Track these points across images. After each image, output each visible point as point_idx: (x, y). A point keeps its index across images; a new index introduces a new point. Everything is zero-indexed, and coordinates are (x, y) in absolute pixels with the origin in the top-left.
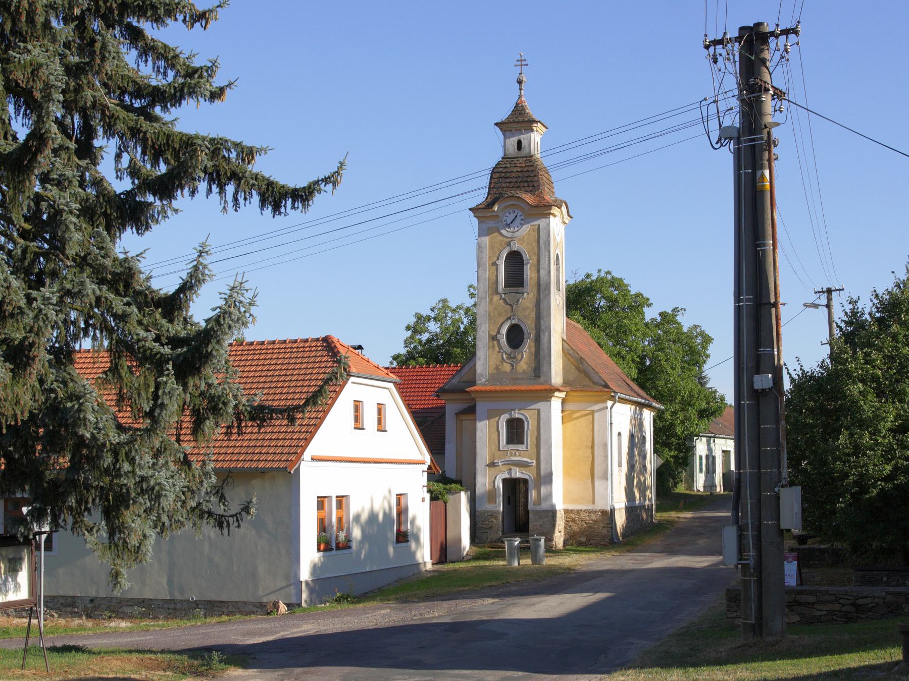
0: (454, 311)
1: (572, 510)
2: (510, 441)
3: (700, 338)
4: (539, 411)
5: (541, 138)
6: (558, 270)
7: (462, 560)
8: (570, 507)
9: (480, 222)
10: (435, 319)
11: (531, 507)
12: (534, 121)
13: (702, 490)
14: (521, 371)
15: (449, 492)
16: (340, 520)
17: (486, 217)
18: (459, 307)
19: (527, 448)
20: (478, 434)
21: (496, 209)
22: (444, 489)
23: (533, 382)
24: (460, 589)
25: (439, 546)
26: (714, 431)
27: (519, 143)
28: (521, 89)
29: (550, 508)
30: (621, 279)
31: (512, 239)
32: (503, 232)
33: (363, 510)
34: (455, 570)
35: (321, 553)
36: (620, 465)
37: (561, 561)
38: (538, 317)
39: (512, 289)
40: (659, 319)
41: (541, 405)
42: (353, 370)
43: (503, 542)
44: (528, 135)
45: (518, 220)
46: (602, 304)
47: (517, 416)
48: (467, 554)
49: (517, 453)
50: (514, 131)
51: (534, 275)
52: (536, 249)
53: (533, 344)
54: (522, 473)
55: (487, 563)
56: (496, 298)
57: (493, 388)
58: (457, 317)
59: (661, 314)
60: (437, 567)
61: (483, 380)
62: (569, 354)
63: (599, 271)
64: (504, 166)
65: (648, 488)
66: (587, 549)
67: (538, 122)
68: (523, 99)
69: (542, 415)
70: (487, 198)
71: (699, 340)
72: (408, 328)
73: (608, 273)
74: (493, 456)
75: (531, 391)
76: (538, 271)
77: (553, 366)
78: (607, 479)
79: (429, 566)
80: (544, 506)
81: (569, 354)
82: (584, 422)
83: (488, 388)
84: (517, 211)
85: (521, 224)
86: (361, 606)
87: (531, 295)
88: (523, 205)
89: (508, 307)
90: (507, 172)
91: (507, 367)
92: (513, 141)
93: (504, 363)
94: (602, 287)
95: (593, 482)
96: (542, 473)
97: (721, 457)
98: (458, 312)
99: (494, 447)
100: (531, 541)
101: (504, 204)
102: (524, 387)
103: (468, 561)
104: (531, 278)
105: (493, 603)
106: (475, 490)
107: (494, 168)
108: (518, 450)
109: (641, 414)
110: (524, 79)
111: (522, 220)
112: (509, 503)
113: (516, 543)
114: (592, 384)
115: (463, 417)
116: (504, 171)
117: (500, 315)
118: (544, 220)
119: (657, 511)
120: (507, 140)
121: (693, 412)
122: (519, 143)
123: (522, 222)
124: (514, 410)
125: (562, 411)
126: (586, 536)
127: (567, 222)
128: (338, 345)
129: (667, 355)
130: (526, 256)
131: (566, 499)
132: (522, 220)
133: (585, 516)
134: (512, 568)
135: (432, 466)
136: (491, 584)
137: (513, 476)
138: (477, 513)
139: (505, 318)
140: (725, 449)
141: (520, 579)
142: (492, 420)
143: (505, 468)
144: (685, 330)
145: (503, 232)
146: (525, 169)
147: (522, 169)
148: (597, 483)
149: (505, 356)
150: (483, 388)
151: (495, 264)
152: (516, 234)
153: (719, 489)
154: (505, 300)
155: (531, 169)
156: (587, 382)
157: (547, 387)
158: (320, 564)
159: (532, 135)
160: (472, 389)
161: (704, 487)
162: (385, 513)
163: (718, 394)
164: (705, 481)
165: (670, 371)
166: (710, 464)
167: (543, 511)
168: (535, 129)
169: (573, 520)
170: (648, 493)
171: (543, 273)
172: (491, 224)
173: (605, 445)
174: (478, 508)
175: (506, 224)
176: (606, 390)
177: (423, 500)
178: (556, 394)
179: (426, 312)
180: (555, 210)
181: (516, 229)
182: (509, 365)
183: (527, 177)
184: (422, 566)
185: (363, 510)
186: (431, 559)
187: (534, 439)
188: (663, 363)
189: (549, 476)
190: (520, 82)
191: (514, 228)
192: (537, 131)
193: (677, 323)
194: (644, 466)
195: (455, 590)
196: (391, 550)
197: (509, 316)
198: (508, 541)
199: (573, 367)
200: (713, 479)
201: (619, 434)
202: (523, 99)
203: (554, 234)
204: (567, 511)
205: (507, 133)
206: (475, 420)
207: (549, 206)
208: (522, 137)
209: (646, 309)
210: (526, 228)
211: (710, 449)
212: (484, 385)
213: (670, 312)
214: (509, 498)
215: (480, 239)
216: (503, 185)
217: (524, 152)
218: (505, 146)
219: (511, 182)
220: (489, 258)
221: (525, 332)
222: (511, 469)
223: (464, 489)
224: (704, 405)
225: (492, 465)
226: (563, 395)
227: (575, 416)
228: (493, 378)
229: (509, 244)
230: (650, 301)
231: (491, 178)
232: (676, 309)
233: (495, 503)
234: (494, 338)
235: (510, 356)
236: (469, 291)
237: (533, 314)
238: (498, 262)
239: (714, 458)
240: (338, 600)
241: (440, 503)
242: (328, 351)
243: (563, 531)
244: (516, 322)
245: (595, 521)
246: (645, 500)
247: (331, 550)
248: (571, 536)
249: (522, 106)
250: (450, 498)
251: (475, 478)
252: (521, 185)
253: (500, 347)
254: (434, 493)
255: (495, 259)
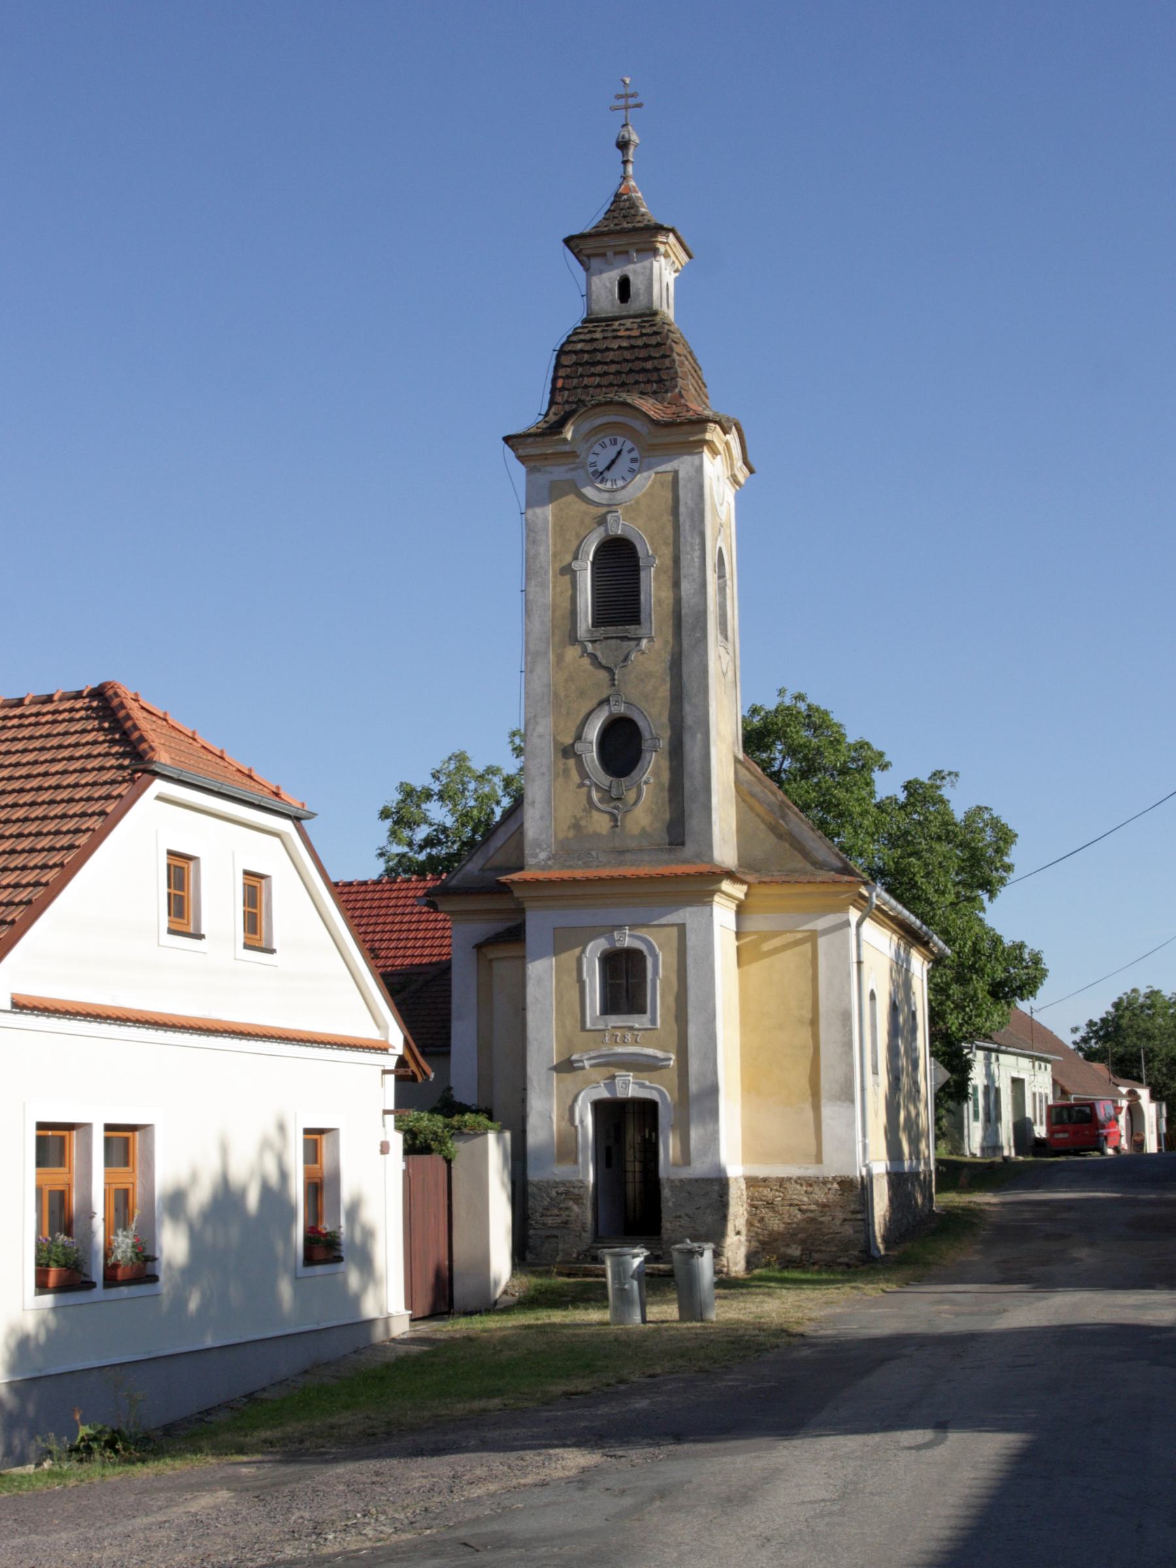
0: (481, 778)
1: (765, 1180)
2: (611, 1006)
3: (989, 831)
4: (682, 928)
5: (676, 280)
6: (722, 590)
7: (490, 1307)
8: (761, 1171)
9: (531, 471)
10: (441, 797)
11: (663, 1173)
12: (659, 229)
13: (978, 1153)
14: (636, 831)
15: (459, 1132)
16: (121, 1201)
17: (545, 457)
18: (492, 771)
19: (653, 1021)
20: (531, 1017)
21: (569, 436)
22: (446, 1126)
23: (665, 856)
24: (478, 1404)
25: (431, 1278)
26: (999, 1041)
27: (624, 285)
28: (625, 162)
29: (713, 1175)
30: (826, 713)
31: (611, 507)
32: (589, 491)
33: (194, 1178)
34: (469, 1339)
35: (48, 1300)
36: (875, 1072)
37: (752, 1308)
38: (677, 697)
39: (611, 630)
40: (902, 797)
41: (687, 915)
42: (163, 758)
43: (597, 1260)
44: (646, 263)
45: (624, 462)
46: (786, 764)
47: (628, 942)
48: (505, 1292)
49: (629, 1036)
50: (610, 254)
51: (667, 594)
52: (669, 530)
53: (665, 764)
54: (642, 1086)
55: (557, 1317)
56: (572, 652)
57: (566, 874)
58: (487, 790)
59: (908, 787)
60: (425, 1328)
61: (543, 855)
62: (753, 795)
63: (781, 692)
64: (588, 337)
65: (923, 1136)
66: (808, 1276)
67: (672, 230)
68: (632, 183)
69: (692, 940)
70: (546, 415)
71: (989, 836)
72: (385, 814)
73: (800, 697)
74: (568, 1044)
75: (663, 878)
76: (676, 584)
77: (715, 817)
78: (852, 1101)
79: (401, 1327)
80: (699, 1168)
81: (753, 795)
82: (792, 960)
83: (555, 874)
84: (620, 440)
85: (632, 471)
86: (144, 1472)
87: (658, 644)
88: (638, 425)
89: (603, 675)
90: (595, 350)
91: (600, 823)
92: (606, 282)
93: (595, 814)
94: (788, 725)
95: (817, 1108)
96: (693, 1087)
97: (1009, 1090)
98: (489, 781)
99: (571, 1023)
100: (675, 1255)
101: (587, 426)
102: (644, 870)
103: (507, 1310)
104: (659, 602)
105: (583, 1479)
106: (524, 1132)
107: (563, 345)
108: (631, 1028)
109: (908, 954)
110: (634, 137)
111: (633, 460)
112: (608, 1164)
113: (637, 1262)
114: (809, 867)
115: (493, 953)
116: (588, 347)
117: (582, 694)
118: (687, 459)
119: (937, 1192)
120: (595, 280)
121: (980, 986)
122: (624, 285)
123: (635, 466)
124: (620, 927)
125: (739, 935)
126: (802, 1242)
127: (742, 480)
128: (137, 714)
129: (926, 865)
130: (645, 547)
131: (750, 1153)
132: (633, 460)
133: (798, 1194)
134: (627, 1332)
135: (408, 1058)
136: (571, 1388)
137: (620, 1094)
138: (531, 1189)
139: (595, 702)
140: (1016, 1075)
141: (659, 1370)
142: (564, 956)
143: (599, 1074)
144: (959, 816)
145: (589, 491)
146: (640, 342)
147: (633, 342)
148: (827, 1111)
149: (595, 795)
150: (541, 875)
151: (568, 571)
152: (620, 496)
153: (1009, 1151)
154: (593, 657)
155: (653, 340)
156: (800, 863)
157: (704, 868)
158: (42, 1338)
159: (656, 265)
160: (515, 876)
161: (983, 1149)
162: (266, 1190)
163: (1027, 951)
164: (984, 1138)
165: (934, 898)
166: (992, 1105)
167: (697, 1180)
168: (662, 248)
169: (770, 1204)
170: (923, 1146)
171: (687, 588)
172: (559, 472)
173: (846, 1016)
174: (534, 1175)
175: (594, 473)
176: (846, 878)
177: (384, 1148)
178: (726, 886)
179: (421, 780)
180: (714, 434)
181: (620, 483)
182: (607, 817)
183: (645, 359)
184: (379, 1334)
185: (194, 1178)
186: (407, 1308)
187: (671, 1000)
188: (919, 880)
189: (712, 1091)
190: (623, 145)
191: (614, 481)
192: (666, 255)
193: (942, 801)
194: (916, 1083)
195: (460, 1408)
196: (285, 1289)
197: (604, 696)
198: (613, 1255)
199: (762, 826)
200: (996, 1133)
201: (873, 996)
202: (632, 183)
203: (712, 497)
204: (751, 1182)
205: (595, 263)
206: (523, 958)
207: (701, 423)
208: (630, 270)
209: (877, 775)
210: (644, 481)
211: (989, 1075)
212: (543, 868)
213: (927, 781)
214: (608, 1150)
215: (530, 512)
216: (586, 381)
217: (637, 304)
218: (588, 295)
219: (606, 374)
220: (555, 555)
221: (646, 734)
222: (613, 1077)
223: (497, 1125)
224: (1000, 975)
225: (566, 1066)
226: (739, 891)
227: (766, 947)
228: (566, 851)
229: (602, 521)
230: (887, 758)
231: (558, 366)
232: (937, 775)
233: (576, 1162)
234: (568, 752)
235: (610, 797)
236: (512, 742)
237: (665, 691)
238: (575, 565)
239: (998, 1091)
240: (82, 1452)
241: (433, 1162)
242: (102, 719)
243: (744, 1231)
244: (620, 709)
245: (824, 1206)
246: (918, 1159)
247: (90, 1285)
248: (762, 1243)
249: (629, 199)
250: (459, 1148)
251: (524, 1101)
252: (631, 379)
253: (584, 775)
254: (421, 1137)
255: (568, 558)
